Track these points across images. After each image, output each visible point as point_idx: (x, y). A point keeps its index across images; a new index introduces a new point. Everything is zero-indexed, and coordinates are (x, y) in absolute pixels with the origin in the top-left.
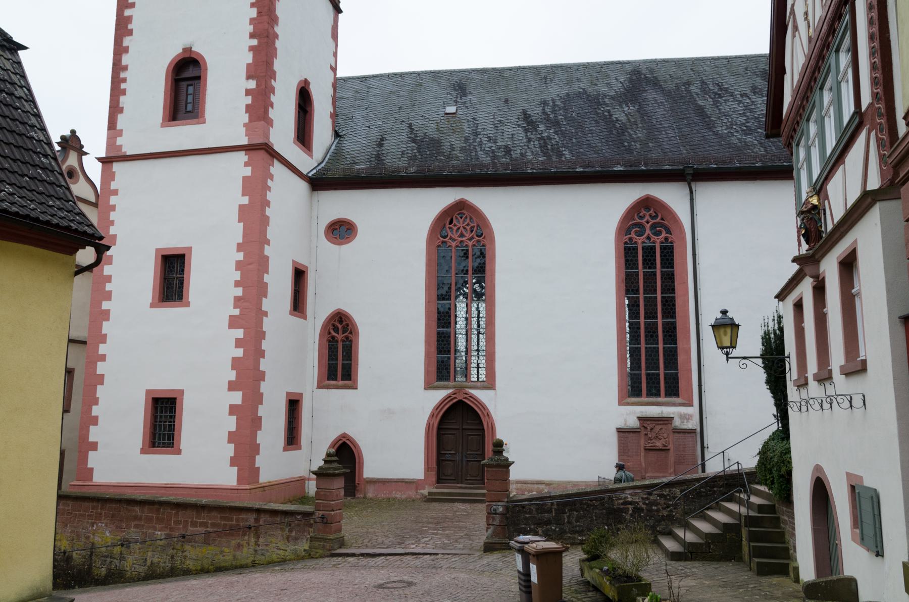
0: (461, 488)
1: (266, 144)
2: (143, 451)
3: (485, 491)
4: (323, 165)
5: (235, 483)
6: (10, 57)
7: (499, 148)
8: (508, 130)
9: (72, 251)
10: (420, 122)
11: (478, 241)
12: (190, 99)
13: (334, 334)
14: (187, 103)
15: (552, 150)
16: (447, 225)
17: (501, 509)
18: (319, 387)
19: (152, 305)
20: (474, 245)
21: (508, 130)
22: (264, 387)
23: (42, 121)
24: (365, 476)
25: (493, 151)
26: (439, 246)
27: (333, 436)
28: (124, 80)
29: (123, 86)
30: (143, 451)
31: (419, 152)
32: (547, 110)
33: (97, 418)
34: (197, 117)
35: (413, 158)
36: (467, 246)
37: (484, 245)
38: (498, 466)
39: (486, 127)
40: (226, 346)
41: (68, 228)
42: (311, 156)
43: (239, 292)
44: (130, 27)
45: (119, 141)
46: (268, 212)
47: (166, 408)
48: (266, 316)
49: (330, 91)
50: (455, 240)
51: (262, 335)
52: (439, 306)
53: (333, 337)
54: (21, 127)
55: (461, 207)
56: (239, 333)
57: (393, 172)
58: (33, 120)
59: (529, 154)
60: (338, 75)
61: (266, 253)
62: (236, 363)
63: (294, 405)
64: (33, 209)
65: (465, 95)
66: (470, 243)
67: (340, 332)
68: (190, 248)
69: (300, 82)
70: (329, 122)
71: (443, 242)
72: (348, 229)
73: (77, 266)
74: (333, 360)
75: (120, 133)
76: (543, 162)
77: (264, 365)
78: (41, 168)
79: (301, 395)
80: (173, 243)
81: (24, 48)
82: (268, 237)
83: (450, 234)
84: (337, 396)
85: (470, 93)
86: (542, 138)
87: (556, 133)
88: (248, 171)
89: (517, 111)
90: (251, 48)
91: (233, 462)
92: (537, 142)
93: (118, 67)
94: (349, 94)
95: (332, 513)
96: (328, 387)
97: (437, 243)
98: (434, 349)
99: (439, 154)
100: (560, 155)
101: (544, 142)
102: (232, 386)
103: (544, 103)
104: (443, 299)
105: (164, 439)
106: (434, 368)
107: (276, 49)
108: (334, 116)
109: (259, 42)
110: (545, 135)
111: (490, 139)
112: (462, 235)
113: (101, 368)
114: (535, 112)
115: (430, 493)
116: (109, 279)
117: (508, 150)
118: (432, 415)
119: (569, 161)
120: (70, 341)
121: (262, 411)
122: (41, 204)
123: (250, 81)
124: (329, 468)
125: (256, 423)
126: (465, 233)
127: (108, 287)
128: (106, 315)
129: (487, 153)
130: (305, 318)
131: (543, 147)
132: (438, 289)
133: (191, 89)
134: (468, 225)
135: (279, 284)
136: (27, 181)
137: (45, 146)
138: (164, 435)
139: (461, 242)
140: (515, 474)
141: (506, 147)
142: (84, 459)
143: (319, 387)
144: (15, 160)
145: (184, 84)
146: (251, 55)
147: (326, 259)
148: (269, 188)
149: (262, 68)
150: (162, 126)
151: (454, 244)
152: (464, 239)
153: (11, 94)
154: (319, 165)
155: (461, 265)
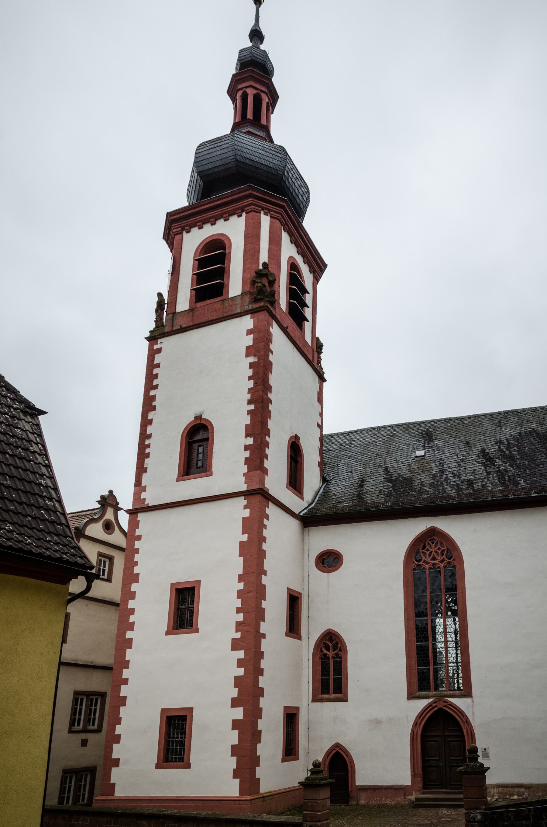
0: (445, 793)
1: (262, 490)
2: (158, 766)
3: (461, 796)
4: (313, 505)
5: (238, 795)
6: (30, 420)
7: (463, 481)
8: (470, 467)
9: (66, 581)
10: (395, 465)
11: (449, 563)
12: (200, 456)
13: (326, 652)
14: (198, 461)
15: (509, 480)
16: (421, 551)
17: (479, 817)
18: (314, 700)
19: (168, 633)
20: (445, 567)
21: (470, 467)
22: (263, 702)
23: (52, 471)
24: (358, 783)
25: (458, 485)
26: (414, 569)
27: (327, 746)
28: (148, 446)
29: (147, 451)
30: (158, 766)
31: (394, 489)
32: (503, 448)
33: (119, 736)
34: (205, 471)
35: (389, 495)
36: (439, 567)
37: (454, 566)
38: (474, 772)
39: (451, 464)
40: (229, 666)
41: (60, 559)
42: (302, 498)
43: (240, 617)
44: (154, 404)
45: (143, 495)
46: (264, 546)
47: (178, 725)
48: (265, 638)
49: (318, 444)
50: (427, 563)
51: (260, 655)
52: (417, 622)
53: (325, 655)
54: (31, 476)
55: (432, 534)
56: (241, 654)
57: (372, 507)
58: (44, 470)
59: (489, 485)
60: (324, 433)
61: (263, 582)
62: (238, 682)
63: (291, 717)
64: (30, 543)
65: (432, 441)
66: (442, 565)
67: (331, 650)
68: (199, 582)
69: (291, 437)
70: (317, 470)
71: (418, 565)
72: (335, 559)
73: (70, 594)
74: (325, 675)
75: (144, 489)
76: (501, 491)
77: (263, 682)
78: (44, 510)
79: (298, 708)
80: (184, 577)
81: (44, 413)
82: (265, 568)
83: (424, 558)
84: (329, 709)
85: (436, 439)
86: (500, 471)
87: (511, 466)
88: (247, 513)
89: (477, 450)
90: (249, 412)
91: (236, 774)
92: (495, 475)
93: (144, 436)
94: (335, 447)
95: (319, 823)
96: (322, 700)
97: (413, 566)
98: (414, 661)
99: (411, 490)
100: (516, 484)
101: (501, 475)
102: (235, 703)
103: (500, 442)
104: (421, 616)
105: (176, 754)
106: (415, 680)
107: (270, 412)
108: (322, 465)
109: (255, 407)
110: (502, 468)
111: (454, 475)
112: (434, 559)
113: (124, 691)
114: (493, 450)
115: (417, 799)
116: (132, 611)
117: (470, 483)
118: (415, 724)
119: (524, 489)
120: (61, 664)
121: (261, 725)
122: (39, 539)
123: (248, 438)
124: (315, 779)
125: (256, 736)
126: (436, 556)
127: (132, 619)
128: (129, 643)
129: (452, 487)
130: (300, 638)
131: (501, 478)
132: (416, 607)
133: (201, 449)
134: (439, 549)
135: (275, 607)
136: (29, 521)
137: (52, 491)
138: (176, 750)
139: (434, 564)
140: (491, 779)
141: (469, 480)
142: (108, 774)
143: (314, 700)
144: (21, 503)
145: (195, 446)
146: (249, 417)
147: (320, 587)
148: (265, 527)
149: (258, 428)
150: (178, 480)
151: (427, 567)
152: (436, 562)
153: (26, 449)
154: (309, 505)
155: (434, 586)
